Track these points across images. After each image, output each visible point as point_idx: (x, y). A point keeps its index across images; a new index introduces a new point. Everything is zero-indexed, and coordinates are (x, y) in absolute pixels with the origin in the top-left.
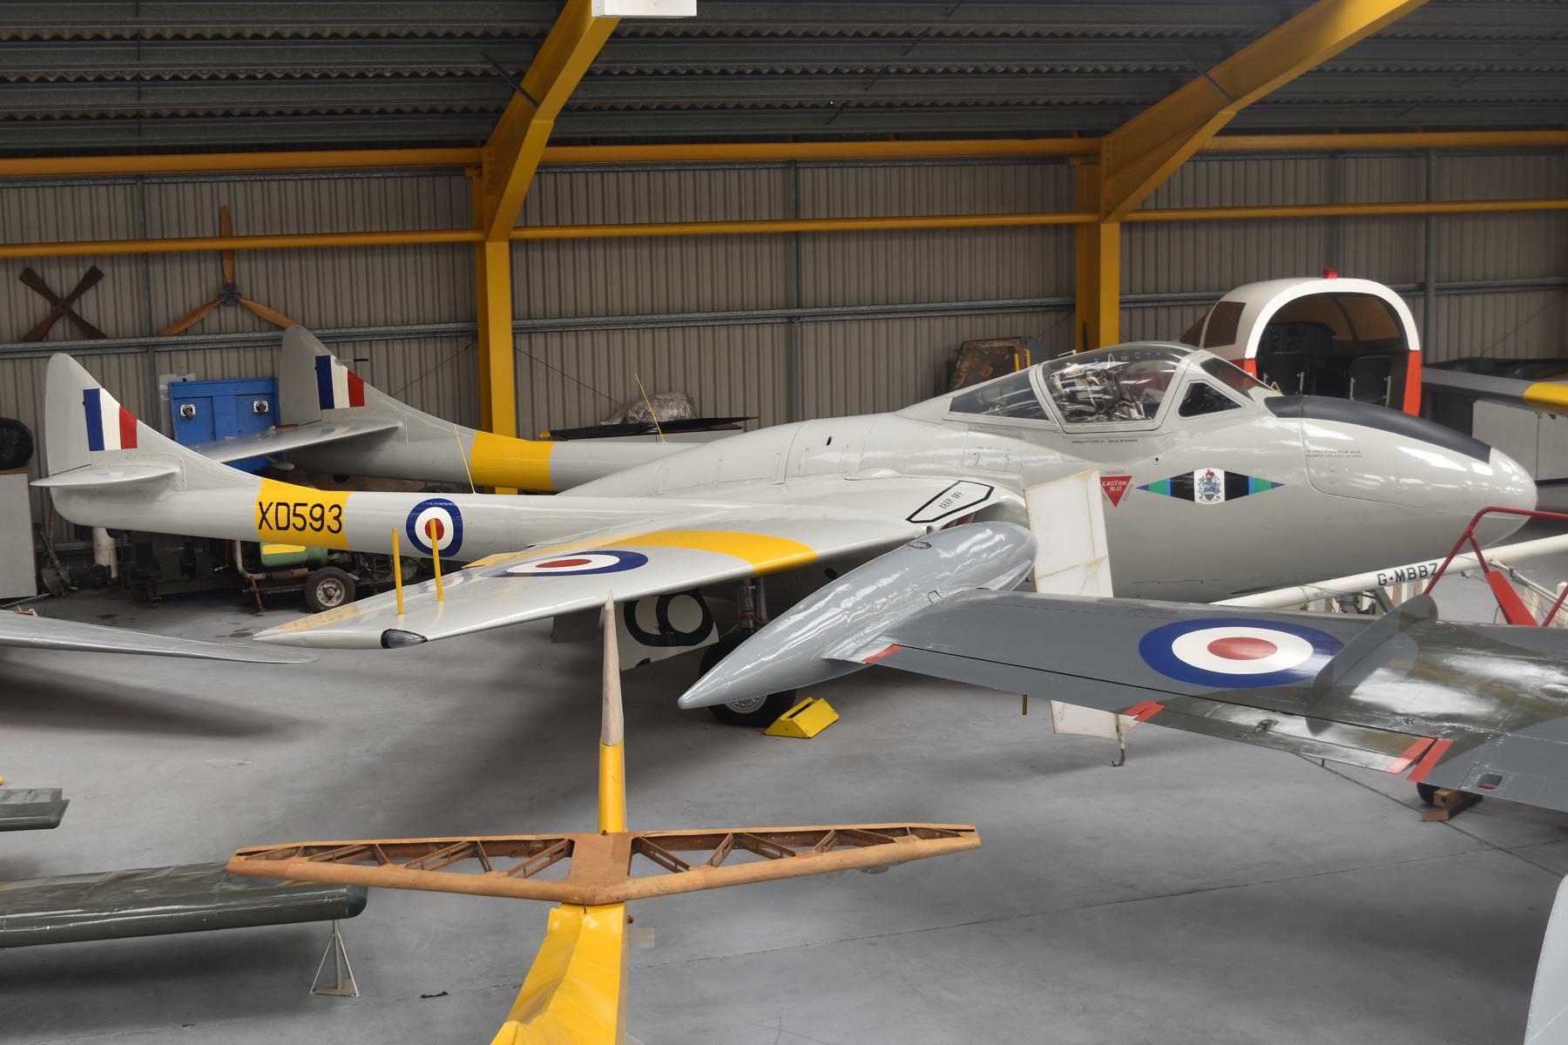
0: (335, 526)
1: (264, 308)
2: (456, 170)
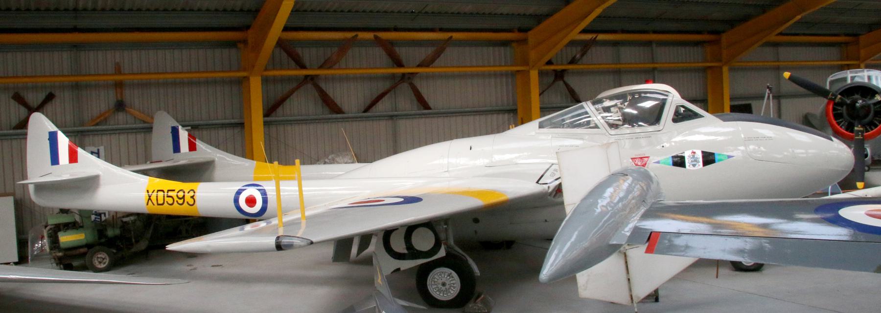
0: (191, 202)
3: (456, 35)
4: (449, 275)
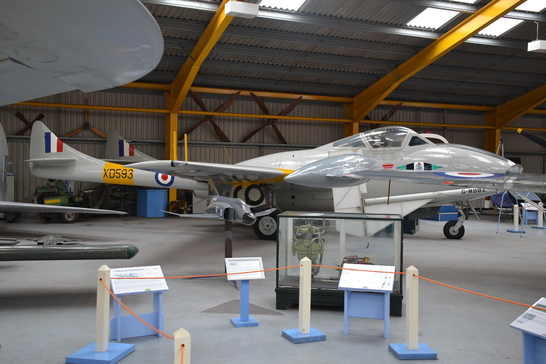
0: (130, 176)
1: (98, 132)
2: (160, 92)
3: (305, 97)
4: (271, 221)
